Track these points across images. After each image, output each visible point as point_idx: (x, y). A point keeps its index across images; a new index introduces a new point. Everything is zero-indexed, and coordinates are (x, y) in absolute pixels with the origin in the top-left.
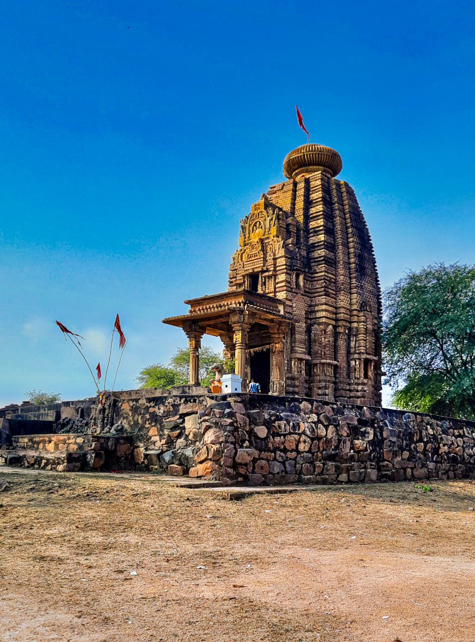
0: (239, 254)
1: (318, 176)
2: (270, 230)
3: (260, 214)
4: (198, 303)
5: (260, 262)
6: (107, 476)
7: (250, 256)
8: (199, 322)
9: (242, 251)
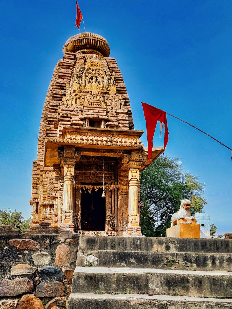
0: (73, 98)
1: (71, 56)
2: (109, 87)
3: (97, 70)
4: (79, 132)
5: (102, 111)
6: (224, 303)
7: (90, 103)
8: (82, 151)
9: (77, 96)
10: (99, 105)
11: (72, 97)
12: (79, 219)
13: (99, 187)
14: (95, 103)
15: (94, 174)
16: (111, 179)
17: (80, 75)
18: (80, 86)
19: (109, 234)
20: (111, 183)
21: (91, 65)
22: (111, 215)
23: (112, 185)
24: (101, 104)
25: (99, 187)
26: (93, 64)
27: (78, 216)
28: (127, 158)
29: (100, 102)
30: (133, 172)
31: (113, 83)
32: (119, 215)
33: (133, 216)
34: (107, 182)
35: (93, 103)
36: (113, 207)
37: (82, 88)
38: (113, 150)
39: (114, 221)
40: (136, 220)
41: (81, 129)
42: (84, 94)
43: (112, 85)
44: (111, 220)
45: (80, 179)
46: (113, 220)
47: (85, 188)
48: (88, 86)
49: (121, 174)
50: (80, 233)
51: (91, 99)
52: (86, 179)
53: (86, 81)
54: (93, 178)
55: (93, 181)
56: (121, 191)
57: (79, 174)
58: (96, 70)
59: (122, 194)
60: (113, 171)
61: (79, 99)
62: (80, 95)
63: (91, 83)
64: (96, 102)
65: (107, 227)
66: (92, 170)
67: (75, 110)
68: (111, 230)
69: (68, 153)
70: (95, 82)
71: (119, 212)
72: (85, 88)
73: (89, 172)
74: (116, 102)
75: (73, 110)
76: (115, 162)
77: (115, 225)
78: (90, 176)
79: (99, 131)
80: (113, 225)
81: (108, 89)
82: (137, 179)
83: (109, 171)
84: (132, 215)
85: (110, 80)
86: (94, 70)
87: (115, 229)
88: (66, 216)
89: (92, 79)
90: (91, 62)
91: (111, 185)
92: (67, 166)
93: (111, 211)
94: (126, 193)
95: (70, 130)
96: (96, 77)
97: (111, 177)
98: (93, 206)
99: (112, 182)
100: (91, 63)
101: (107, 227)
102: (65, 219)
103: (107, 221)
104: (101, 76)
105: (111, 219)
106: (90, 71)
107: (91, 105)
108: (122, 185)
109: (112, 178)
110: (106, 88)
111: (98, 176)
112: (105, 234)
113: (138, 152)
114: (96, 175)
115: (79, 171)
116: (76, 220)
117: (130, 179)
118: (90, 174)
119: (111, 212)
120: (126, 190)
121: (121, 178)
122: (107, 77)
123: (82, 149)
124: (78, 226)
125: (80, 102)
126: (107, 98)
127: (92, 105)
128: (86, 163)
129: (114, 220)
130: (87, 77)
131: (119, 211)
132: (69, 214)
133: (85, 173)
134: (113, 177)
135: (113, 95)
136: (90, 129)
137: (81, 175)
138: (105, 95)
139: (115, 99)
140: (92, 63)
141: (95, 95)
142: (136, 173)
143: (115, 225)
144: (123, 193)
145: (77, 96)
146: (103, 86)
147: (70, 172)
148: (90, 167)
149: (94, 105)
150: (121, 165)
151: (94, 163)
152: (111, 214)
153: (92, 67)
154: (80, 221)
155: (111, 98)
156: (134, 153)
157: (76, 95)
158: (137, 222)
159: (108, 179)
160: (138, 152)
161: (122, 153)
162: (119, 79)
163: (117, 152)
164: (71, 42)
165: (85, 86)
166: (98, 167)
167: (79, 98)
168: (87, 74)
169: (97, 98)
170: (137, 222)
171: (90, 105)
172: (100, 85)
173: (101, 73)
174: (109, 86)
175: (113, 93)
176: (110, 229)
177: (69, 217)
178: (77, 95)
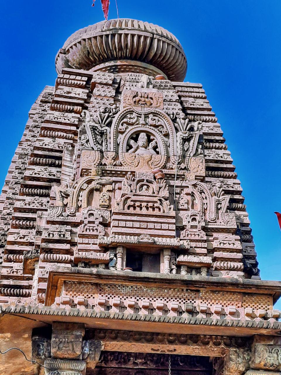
3: (151, 116)
7: (129, 203)
9: (93, 185)
11: (78, 186)
14: (144, 204)
17: (103, 129)
18: (102, 157)
21: (133, 103)
24: (161, 206)
26: (140, 100)
28: (240, 360)
29: (159, 202)
31: (197, 150)
35: (137, 204)
42: (114, 179)
43: (192, 155)
48: (124, 157)
51: (134, 191)
53: (118, 145)
58: (146, 116)
61: (98, 192)
62: (100, 181)
63: (132, 150)
64: (148, 202)
67: (86, 222)
72: (117, 162)
74: (205, 201)
75: (82, 222)
76: (204, 369)
81: (183, 166)
85: (187, 143)
86: (143, 116)
89: (136, 140)
95: (72, 279)
100: (134, 97)
104: (161, 132)
106: (130, 118)
110: (177, 163)
113: (272, 343)
122: (179, 133)
123: (105, 333)
125: (102, 200)
126: (178, 190)
130: (122, 133)
135: (195, 182)
139: (201, 193)
140: (137, 99)
141: (145, 182)
145: (93, 185)
146: (168, 158)
155: (190, 190)
156: (260, 347)
157: (89, 182)
160: (272, 343)
161: (226, 344)
162: (213, 138)
163: (207, 343)
164: (80, 43)
165: (116, 158)
167: (97, 190)
168: (122, 125)
174: (184, 157)
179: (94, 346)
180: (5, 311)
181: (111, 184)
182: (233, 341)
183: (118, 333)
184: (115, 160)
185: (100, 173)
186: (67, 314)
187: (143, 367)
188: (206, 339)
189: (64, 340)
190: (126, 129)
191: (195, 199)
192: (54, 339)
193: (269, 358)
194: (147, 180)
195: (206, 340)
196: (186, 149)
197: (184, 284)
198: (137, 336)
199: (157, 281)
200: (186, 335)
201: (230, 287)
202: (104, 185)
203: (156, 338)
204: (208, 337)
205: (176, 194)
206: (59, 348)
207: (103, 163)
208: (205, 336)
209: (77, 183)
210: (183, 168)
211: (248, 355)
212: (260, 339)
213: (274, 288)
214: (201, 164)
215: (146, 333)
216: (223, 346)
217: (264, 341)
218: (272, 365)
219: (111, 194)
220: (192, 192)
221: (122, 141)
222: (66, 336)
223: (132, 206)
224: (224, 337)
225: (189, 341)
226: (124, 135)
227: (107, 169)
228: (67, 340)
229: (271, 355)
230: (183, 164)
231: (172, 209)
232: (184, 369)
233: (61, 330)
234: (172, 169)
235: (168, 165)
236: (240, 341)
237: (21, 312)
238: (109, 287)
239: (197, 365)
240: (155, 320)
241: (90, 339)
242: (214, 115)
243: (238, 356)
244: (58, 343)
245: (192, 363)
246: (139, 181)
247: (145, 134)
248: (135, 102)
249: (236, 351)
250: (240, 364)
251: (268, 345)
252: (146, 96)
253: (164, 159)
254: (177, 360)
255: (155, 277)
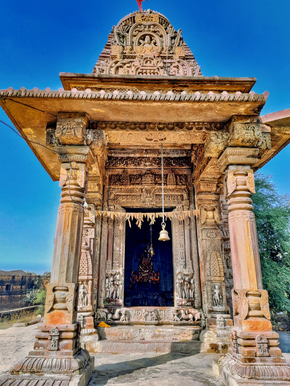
3: (152, 26)
7: (139, 71)
9: (118, 64)
10: (156, 74)
11: (109, 65)
12: (120, 283)
13: (159, 216)
14: (148, 71)
15: (148, 191)
16: (182, 199)
17: (124, 34)
18: (124, 49)
19: (183, 316)
20: (183, 206)
21: (141, 20)
22: (186, 272)
23: (185, 211)
24: (158, 72)
25: (159, 216)
26: (145, 19)
27: (118, 277)
28: (219, 140)
29: (157, 69)
30: (236, 173)
31: (179, 44)
32: (202, 273)
33: (250, 297)
34: (175, 205)
35: (144, 71)
36: (188, 255)
37: (126, 52)
38: (182, 125)
39: (193, 285)
40: (259, 309)
41: (104, 80)
43: (176, 45)
44: (185, 283)
45: (123, 200)
46: (190, 283)
47: (131, 217)
48: (137, 48)
49: (202, 188)
50: (120, 314)
51: (142, 64)
52: (135, 201)
53: (133, 43)
54: (147, 199)
55: (148, 205)
56: (203, 223)
57: (121, 192)
58: (149, 27)
59: (206, 227)
60: (184, 185)
61: (121, 68)
62: (122, 62)
63: (142, 45)
64: (150, 70)
65: (177, 298)
66: (145, 185)
68: (188, 306)
69: (64, 131)
70: (150, 44)
71: (202, 266)
72: (133, 52)
73: (140, 187)
74: (185, 70)
76: (188, 167)
77: (194, 293)
78: (141, 195)
79: (147, 83)
80: (191, 295)
81: (171, 52)
82: (249, 191)
83: (177, 184)
84: (247, 295)
85: (173, 40)
86: (147, 27)
87: (195, 303)
88: (55, 302)
89: (144, 40)
90: (141, 16)
91: (182, 211)
92: (68, 165)
93: (184, 263)
94: (213, 225)
95: (79, 84)
96: (151, 36)
97: (182, 196)
98: (151, 248)
99: (183, 204)
100: (142, 17)
101: (179, 298)
102: (52, 309)
103: (178, 284)
104: (158, 35)
105: (184, 281)
106: (140, 28)
107: (141, 74)
108: (205, 210)
109: (183, 198)
110: (168, 50)
111: (156, 195)
112: (174, 315)
113: (248, 121)
114: (152, 192)
115: (120, 187)
116: (114, 284)
117: (230, 192)
118: (142, 192)
119: (186, 265)
120: (213, 220)
121: (202, 196)
122: (168, 35)
123: (106, 124)
124: (116, 297)
125: (124, 72)
126: (169, 65)
127: (143, 74)
128: (134, 172)
129: (192, 282)
130: (135, 36)
131: (202, 264)
132: (64, 295)
133: (131, 191)
134: (185, 196)
135: (179, 60)
136: (124, 78)
137: (124, 194)
138: (165, 61)
139: (183, 66)
140: (144, 18)
141: (149, 59)
142: (246, 177)
143: (194, 293)
144: (207, 225)
145: (118, 64)
146: (163, 48)
147: (75, 179)
148: (142, 179)
149: (147, 74)
150: (201, 171)
151: (149, 172)
152: (184, 270)
153: (144, 23)
154: (121, 286)
155: (177, 64)
156: (238, 125)
157: (116, 63)
158: (264, 317)
159: (176, 200)
160: (248, 121)
161: (206, 129)
162: (188, 57)
163: (191, 128)
165: (132, 49)
166: (156, 179)
167: (121, 67)
168: (135, 31)
169: (152, 63)
170: (264, 317)
171: (139, 73)
172: (157, 47)
173: (159, 30)
174: (172, 47)
175: (179, 57)
176: (183, 303)
177: (64, 302)
178: (118, 63)
179: (97, 135)
180: (3, 95)
181: (129, 63)
182: (213, 125)
183: (117, 124)
184: (131, 50)
185: (122, 57)
186: (61, 96)
187: (150, 168)
188: (190, 125)
189: (67, 126)
190: (137, 34)
191: (179, 70)
192: (59, 126)
193: (247, 134)
194: (150, 58)
195: (190, 126)
196: (173, 43)
197: (171, 83)
198: (133, 126)
199: (149, 81)
200: (173, 124)
201: (208, 84)
202: (124, 64)
203: (148, 126)
204: (191, 123)
205: (168, 67)
206: (62, 133)
207: (124, 52)
208: (189, 123)
209: (109, 63)
210: (171, 53)
211: (227, 135)
212: (237, 119)
213: (245, 83)
214: (182, 50)
215: (140, 123)
216: (204, 130)
217: (242, 119)
218: (249, 141)
219: (129, 69)
220: (178, 66)
221: (135, 40)
222: (69, 123)
223: (141, 72)
224: (205, 123)
225: (176, 127)
226: (136, 37)
227: (127, 55)
228: (69, 126)
229: (248, 132)
230: (171, 51)
231: (165, 73)
232: (176, 168)
233: (64, 118)
234: (165, 54)
235: (163, 52)
236: (218, 125)
237: (18, 96)
238: (111, 91)
239: (183, 164)
240: (142, 99)
241: (93, 129)
242: (189, 48)
243: (218, 138)
244: (62, 129)
245: (181, 163)
246: (145, 59)
247: (149, 36)
248: (143, 19)
249: (216, 134)
250: (219, 144)
251: (245, 123)
252: (149, 16)
253: (160, 49)
254: (171, 162)
255: (146, 78)
